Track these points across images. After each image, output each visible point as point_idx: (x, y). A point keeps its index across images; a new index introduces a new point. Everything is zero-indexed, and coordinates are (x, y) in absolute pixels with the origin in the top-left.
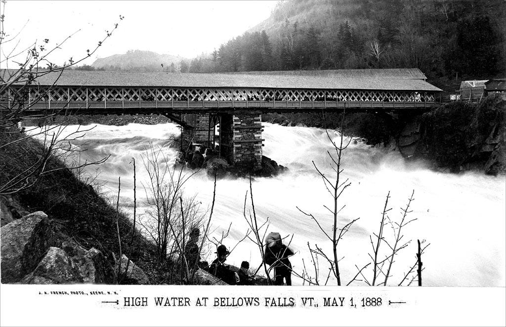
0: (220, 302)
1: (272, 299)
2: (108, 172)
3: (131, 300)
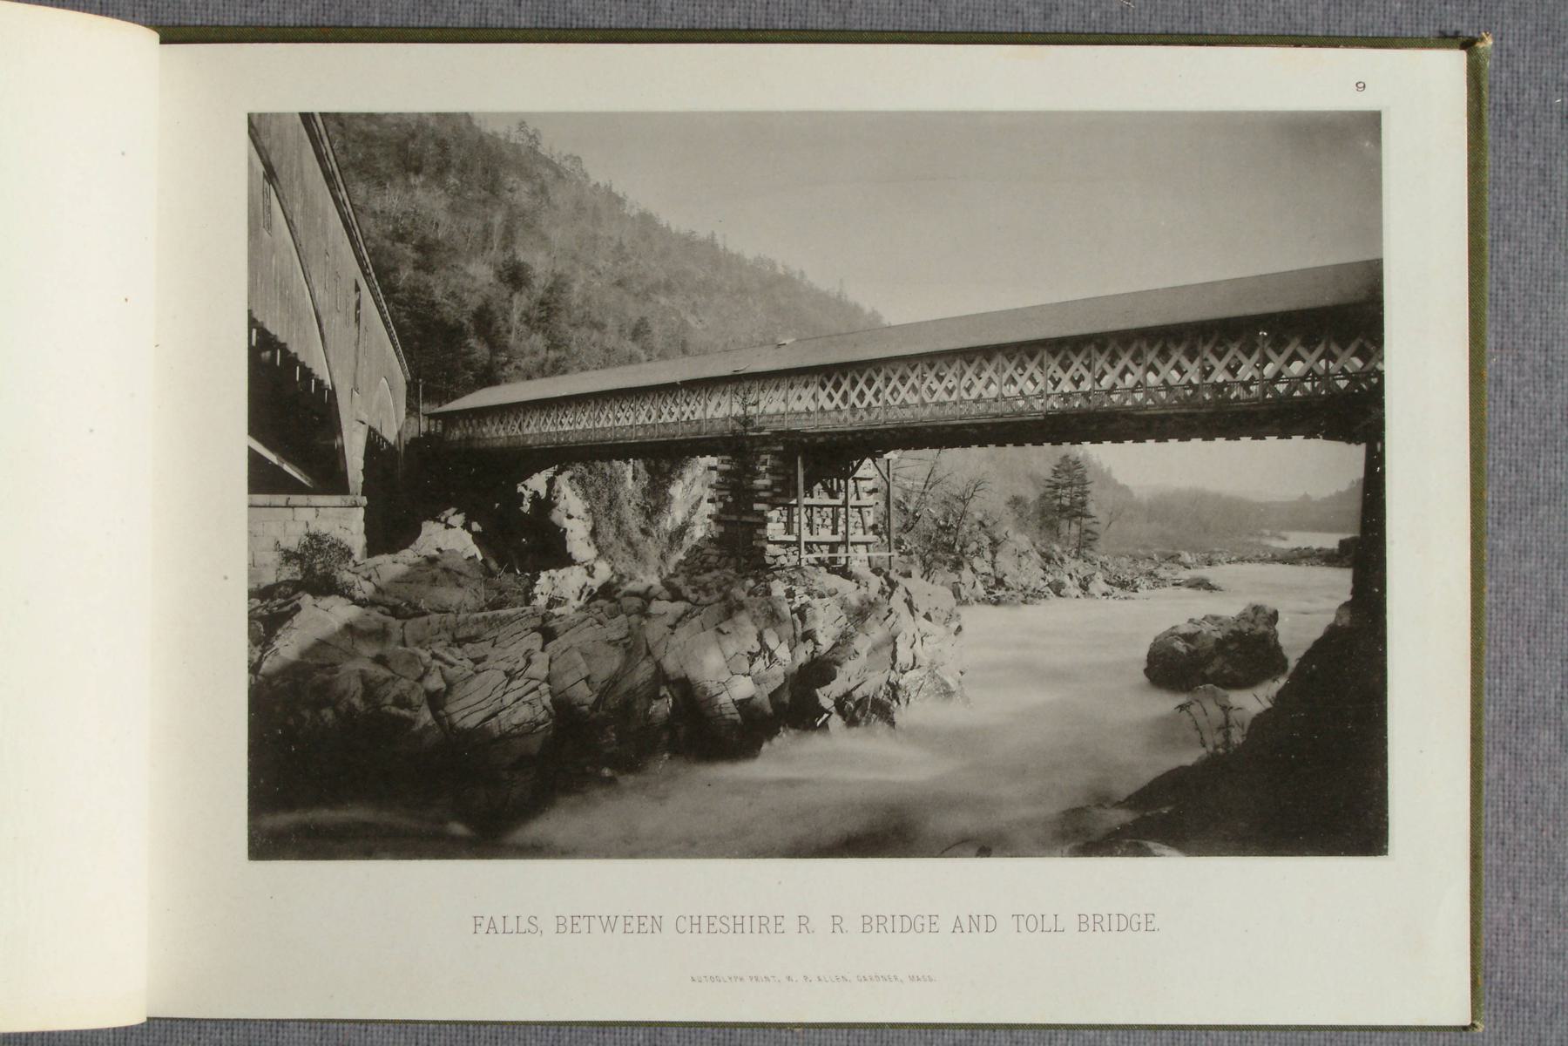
0: (569, 924)
1: (487, 920)
2: (572, 800)
3: (747, 921)
